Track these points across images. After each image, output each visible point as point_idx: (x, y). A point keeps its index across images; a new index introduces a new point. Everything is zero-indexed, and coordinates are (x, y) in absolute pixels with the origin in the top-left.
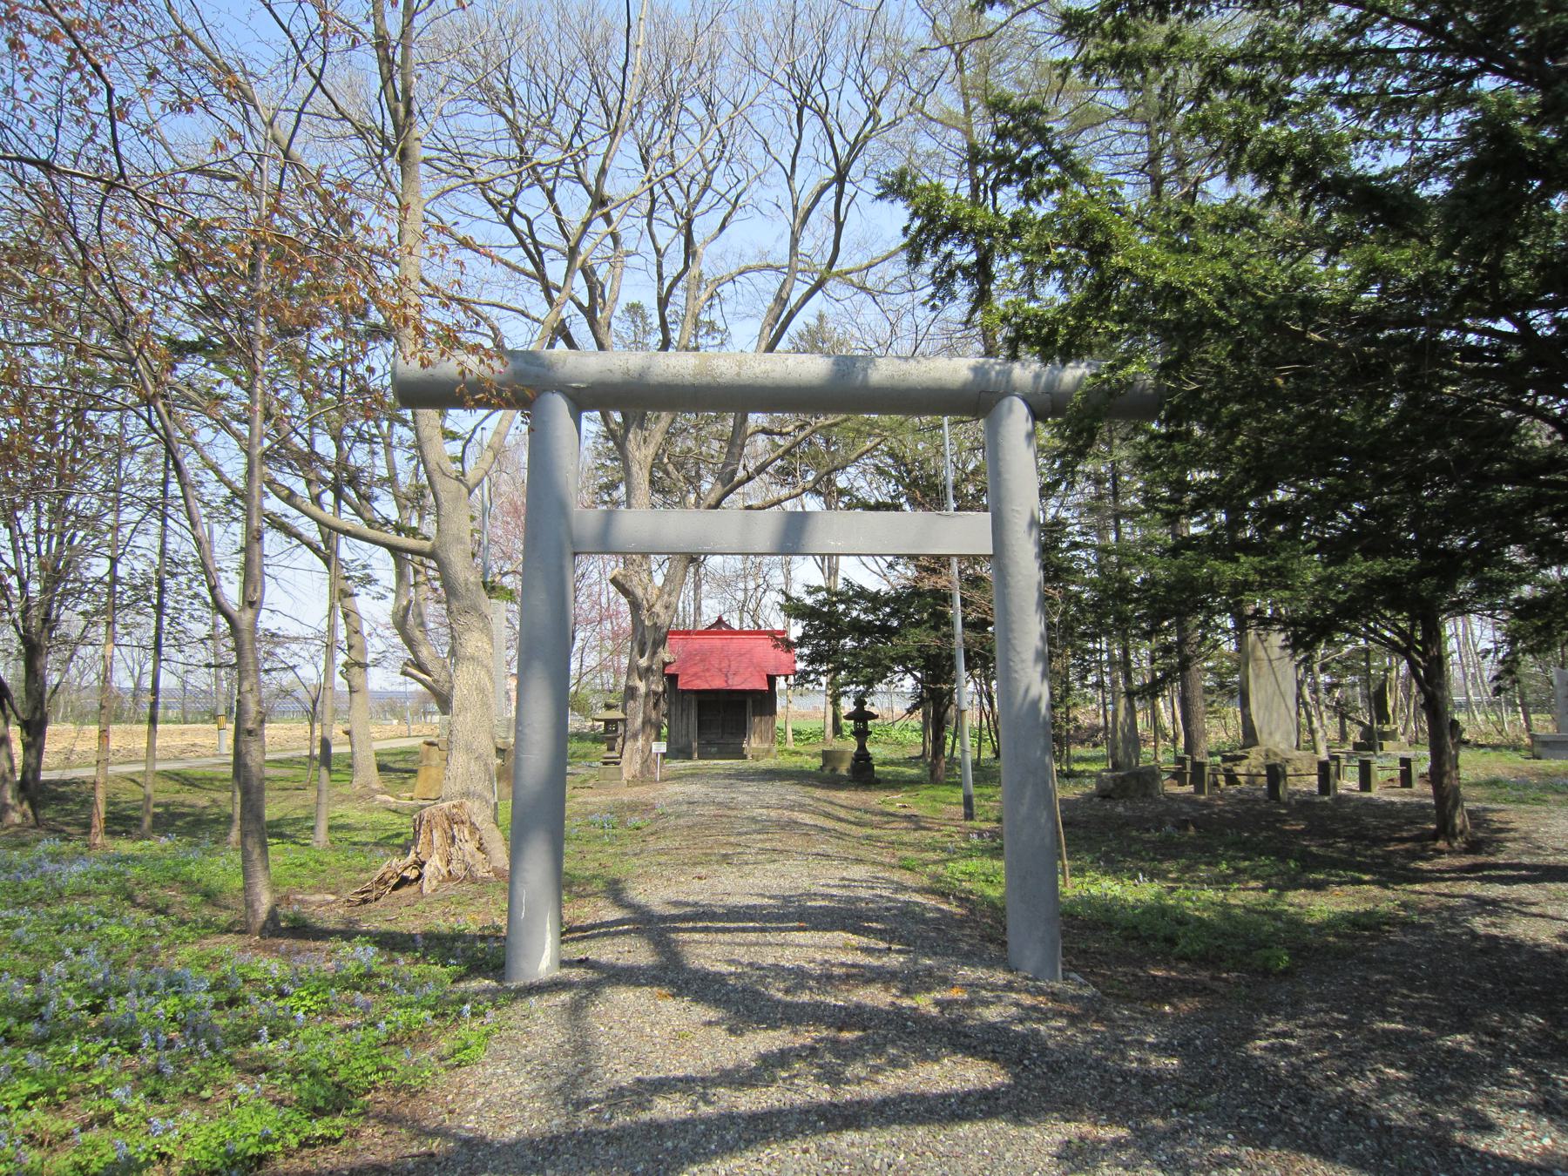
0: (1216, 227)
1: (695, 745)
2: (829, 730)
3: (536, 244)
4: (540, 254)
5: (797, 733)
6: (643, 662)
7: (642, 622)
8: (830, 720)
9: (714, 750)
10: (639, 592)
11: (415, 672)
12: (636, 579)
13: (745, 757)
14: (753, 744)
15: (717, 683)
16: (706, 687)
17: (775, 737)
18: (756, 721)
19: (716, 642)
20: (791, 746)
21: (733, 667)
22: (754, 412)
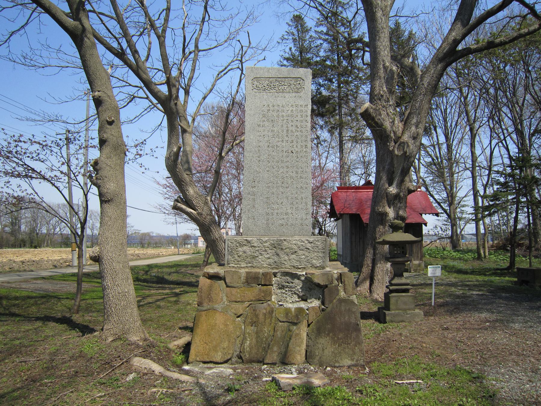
10: (387, 124)
11: (184, 207)
12: (384, 113)
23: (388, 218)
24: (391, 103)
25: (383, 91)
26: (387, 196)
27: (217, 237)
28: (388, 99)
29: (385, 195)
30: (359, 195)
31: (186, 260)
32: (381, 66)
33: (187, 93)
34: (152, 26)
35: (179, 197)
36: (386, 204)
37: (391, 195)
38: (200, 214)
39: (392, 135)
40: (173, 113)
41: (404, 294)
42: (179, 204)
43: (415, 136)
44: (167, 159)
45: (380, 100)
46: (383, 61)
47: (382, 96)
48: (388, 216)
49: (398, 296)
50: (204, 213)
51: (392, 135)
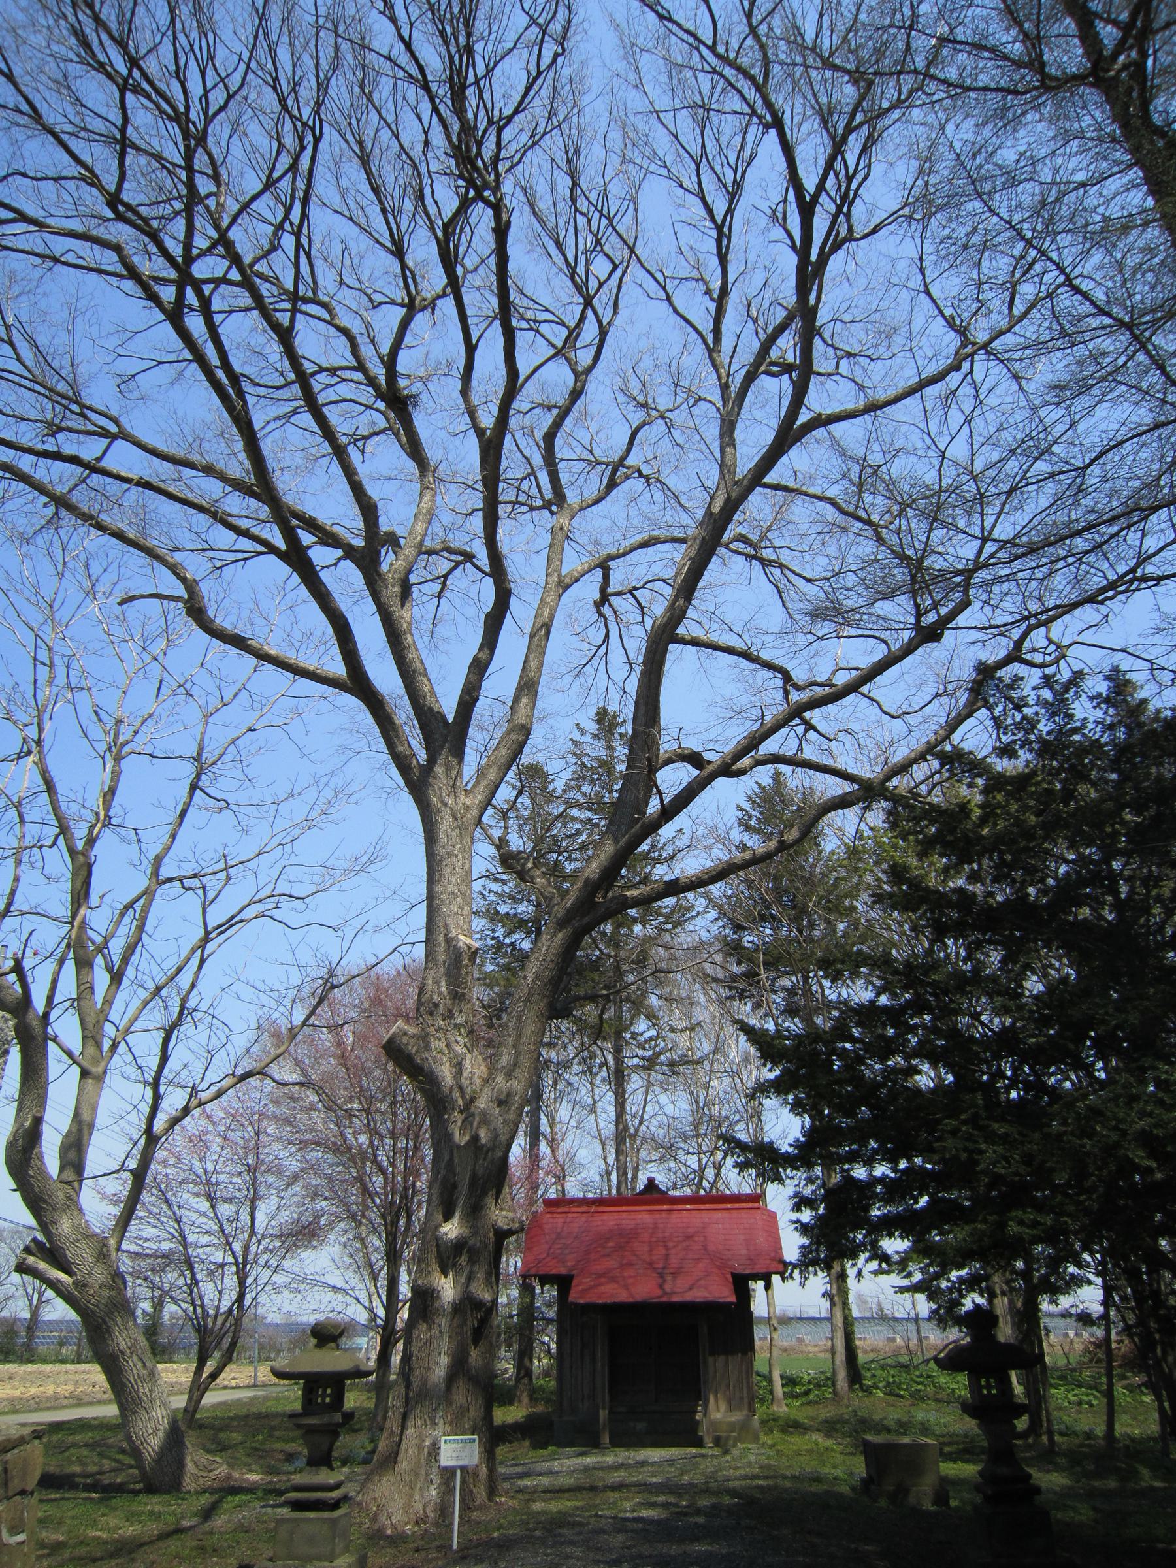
0: (1091, 698)
1: (603, 1414)
2: (842, 1375)
3: (234, 378)
4: (241, 394)
5: (790, 1381)
6: (451, 1230)
7: (449, 1136)
8: (841, 1356)
9: (641, 1426)
10: (445, 1073)
11: (42, 1265)
12: (437, 1044)
13: (699, 1443)
14: (717, 1412)
15: (643, 1290)
16: (622, 1296)
17: (750, 1394)
18: (717, 1366)
19: (643, 1216)
20: (781, 1409)
21: (674, 1261)
22: (860, 1180)
23: (437, 1304)
24: (458, 1021)
25: (440, 993)
26: (438, 1246)
27: (123, 1345)
28: (450, 1011)
29: (434, 1243)
30: (597, 1220)
31: (266, 1398)
32: (441, 938)
33: (117, 978)
34: (64, 830)
35: (35, 1240)
36: (435, 1267)
37: (446, 1243)
38: (81, 1285)
39: (456, 1095)
40: (33, 1038)
41: (312, 1515)
42: (31, 1260)
43: (502, 1097)
44: (11, 1145)
45: (431, 1013)
46: (446, 926)
47: (436, 1005)
48: (438, 1297)
49: (295, 1520)
50: (91, 1281)
51: (456, 1095)
